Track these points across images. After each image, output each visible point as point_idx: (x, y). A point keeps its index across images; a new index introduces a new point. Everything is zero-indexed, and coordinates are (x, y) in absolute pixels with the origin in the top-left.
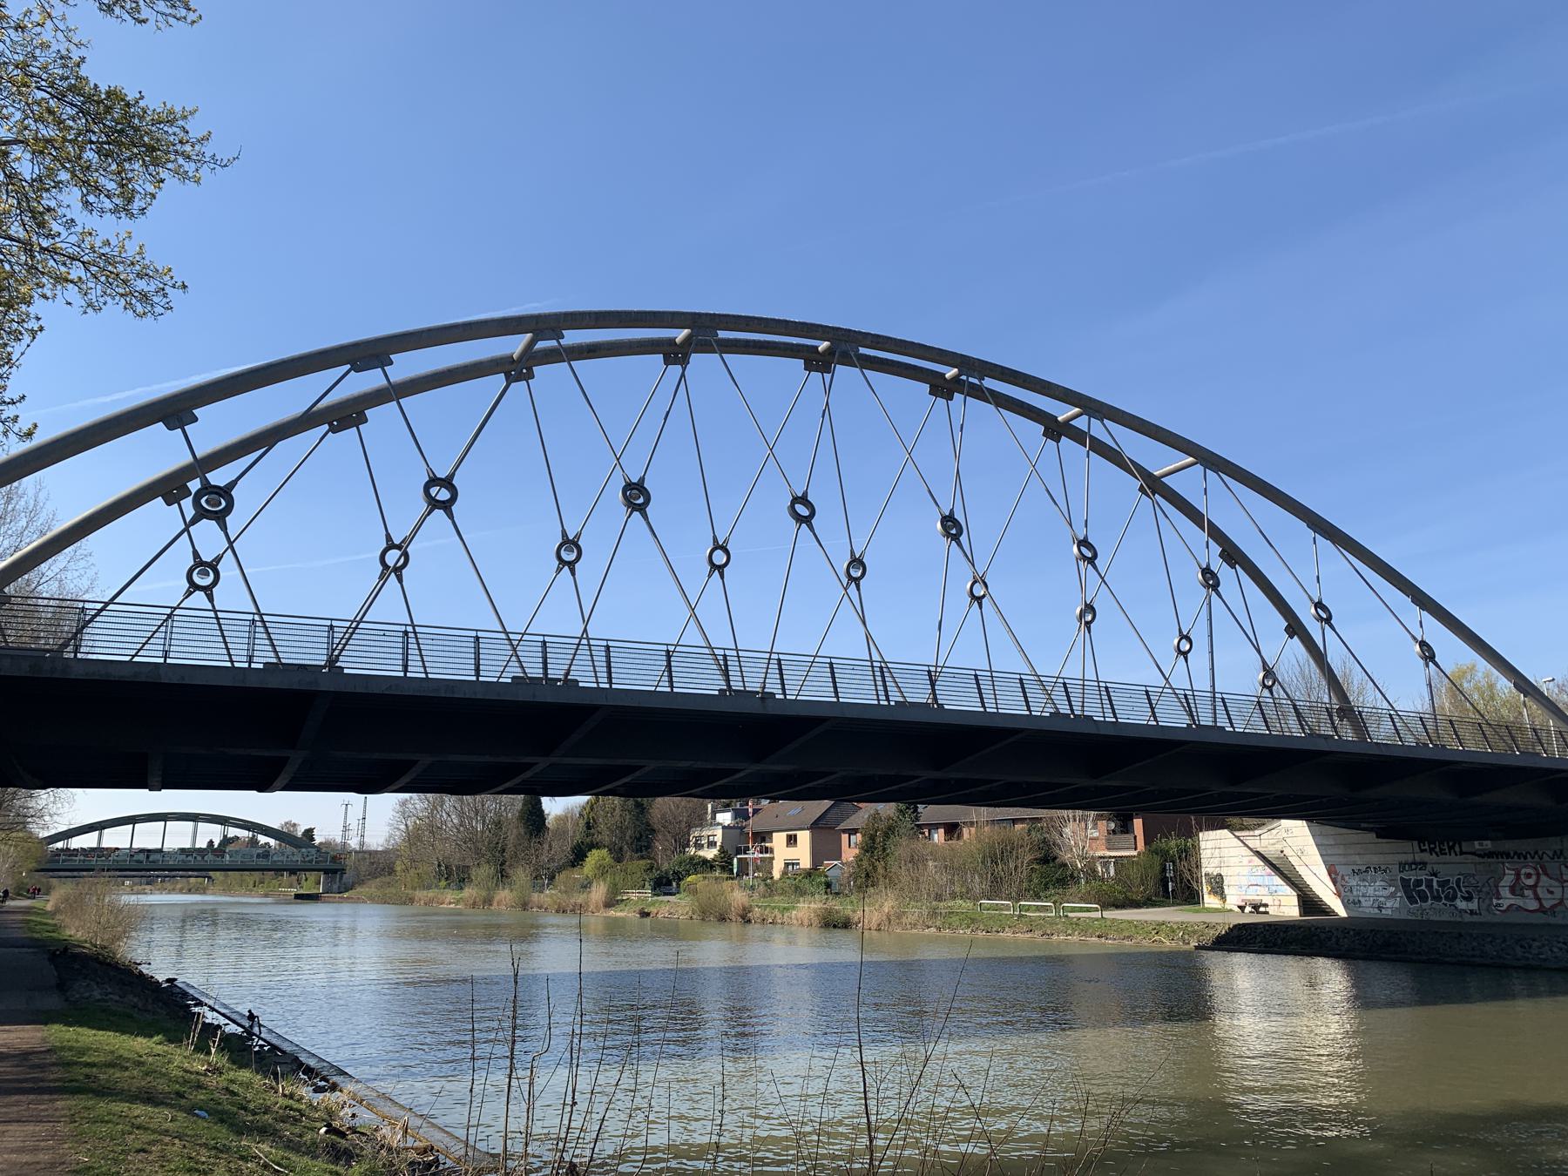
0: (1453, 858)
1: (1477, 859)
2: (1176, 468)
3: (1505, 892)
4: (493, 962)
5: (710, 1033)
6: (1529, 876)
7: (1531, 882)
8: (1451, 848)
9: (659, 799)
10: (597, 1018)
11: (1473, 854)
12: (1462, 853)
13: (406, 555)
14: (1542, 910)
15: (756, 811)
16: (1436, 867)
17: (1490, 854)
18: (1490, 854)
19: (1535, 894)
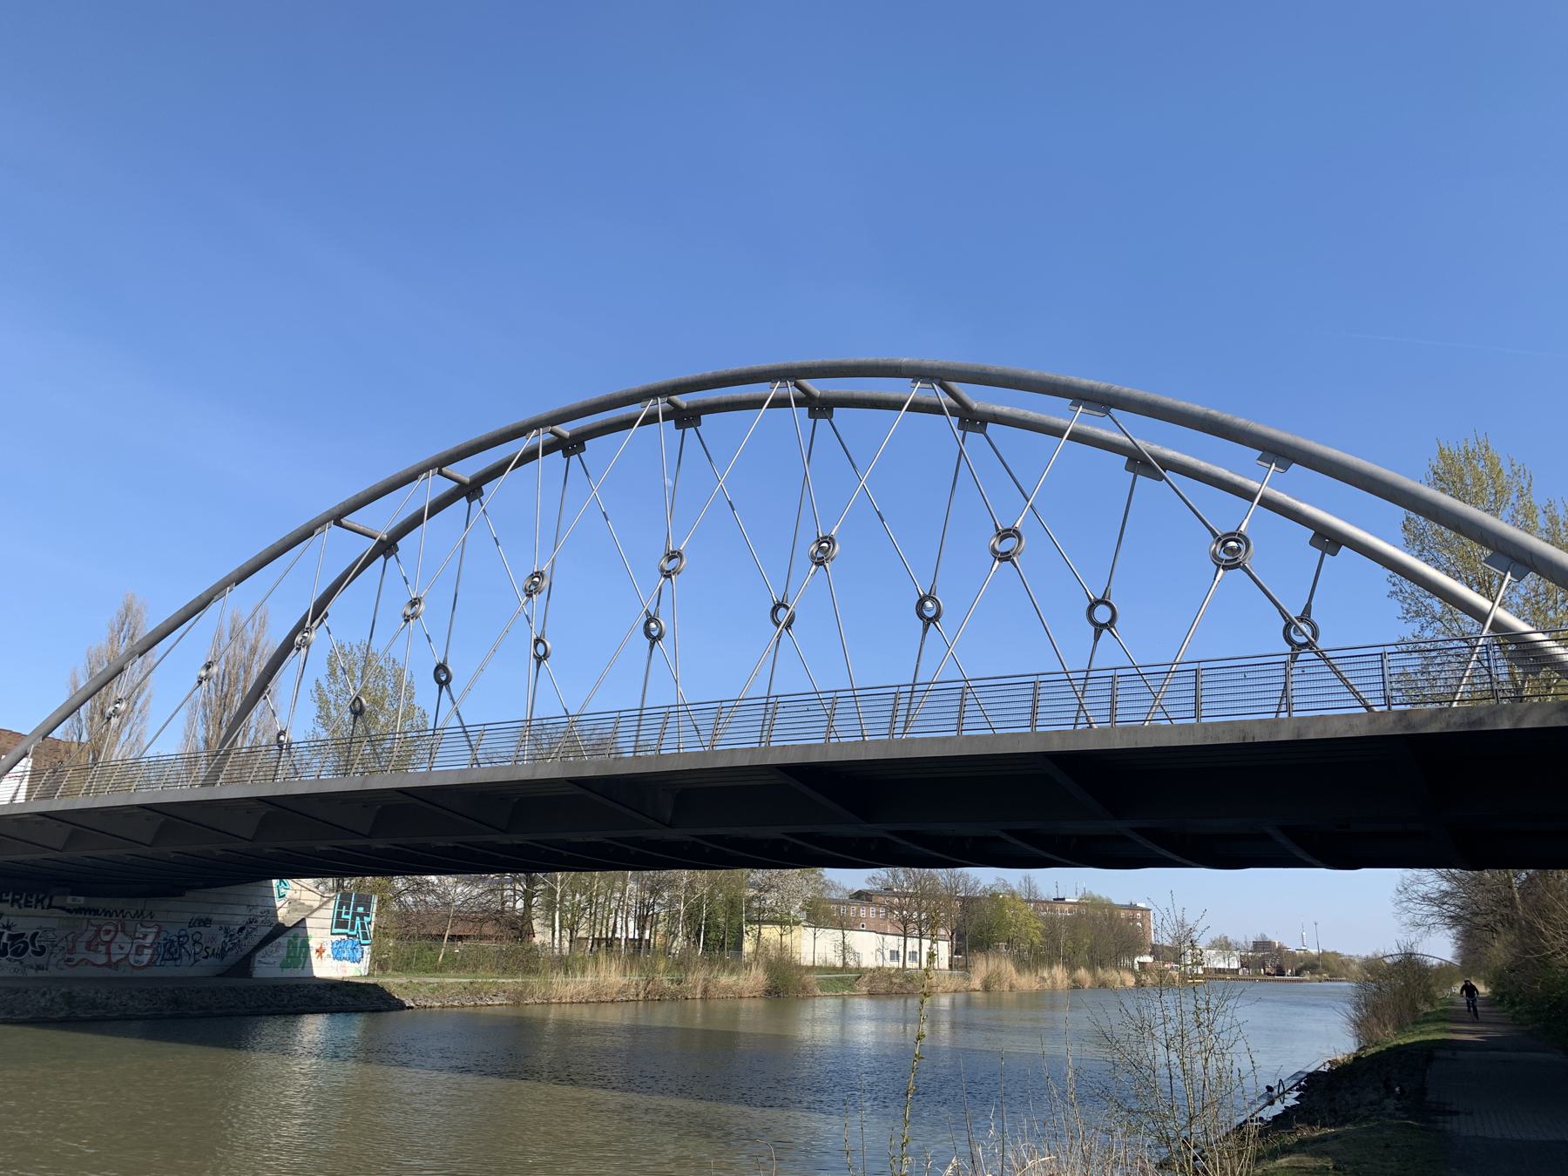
0: (39, 911)
1: (64, 914)
2: (1135, 431)
3: (81, 947)
4: (977, 1041)
5: (309, 1064)
6: (108, 932)
7: (107, 938)
8: (38, 901)
9: (369, 878)
10: (1212, 1073)
11: (63, 908)
12: (50, 906)
13: (921, 615)
14: (109, 964)
15: (1535, 982)
16: (12, 920)
17: (79, 910)
18: (79, 910)
19: (108, 949)
